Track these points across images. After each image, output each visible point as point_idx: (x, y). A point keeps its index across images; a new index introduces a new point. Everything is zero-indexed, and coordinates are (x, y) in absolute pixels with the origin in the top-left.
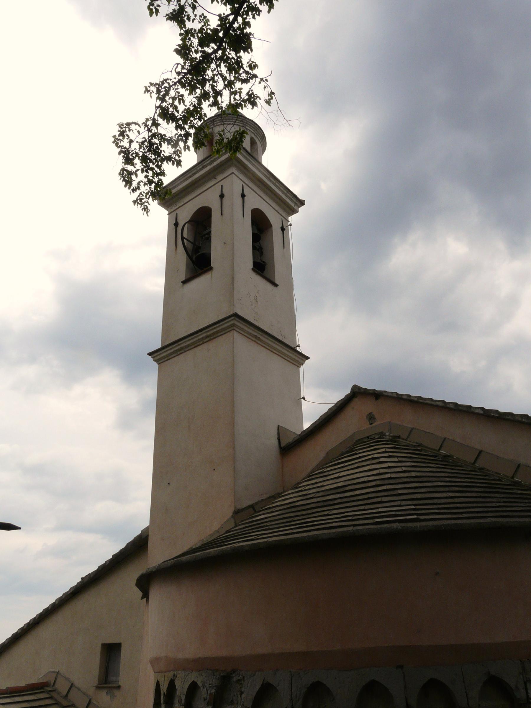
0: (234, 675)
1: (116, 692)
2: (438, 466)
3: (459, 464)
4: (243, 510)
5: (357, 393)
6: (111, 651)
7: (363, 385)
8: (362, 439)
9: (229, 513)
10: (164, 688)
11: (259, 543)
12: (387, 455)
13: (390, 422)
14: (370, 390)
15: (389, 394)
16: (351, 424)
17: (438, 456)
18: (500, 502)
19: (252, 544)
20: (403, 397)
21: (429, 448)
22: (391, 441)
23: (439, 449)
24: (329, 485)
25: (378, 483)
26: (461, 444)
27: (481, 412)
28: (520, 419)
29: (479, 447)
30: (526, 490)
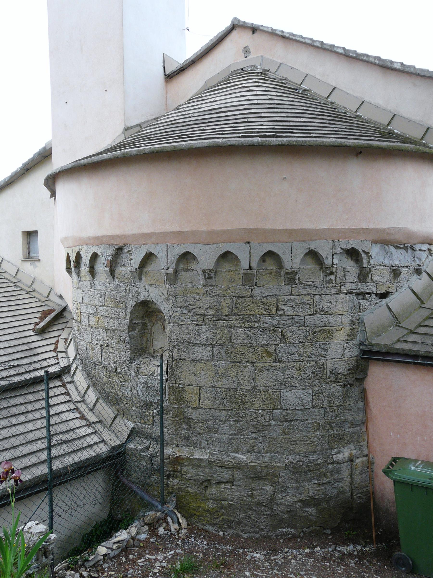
0: (125, 248)
1: (37, 263)
2: (297, 97)
3: (315, 98)
4: (132, 128)
5: (235, 26)
6: (30, 235)
7: (242, 19)
8: (237, 70)
9: (120, 129)
10: (73, 258)
11: (145, 149)
12: (257, 84)
13: (262, 56)
14: (248, 23)
15: (265, 29)
16: (228, 57)
17: (299, 90)
18: (342, 128)
19: (139, 150)
20: (277, 32)
21: (293, 82)
22: (262, 73)
23: (301, 84)
24: (206, 107)
25: (247, 107)
26: (320, 80)
27: (342, 51)
28: (373, 61)
29: (334, 85)
30: (364, 122)
